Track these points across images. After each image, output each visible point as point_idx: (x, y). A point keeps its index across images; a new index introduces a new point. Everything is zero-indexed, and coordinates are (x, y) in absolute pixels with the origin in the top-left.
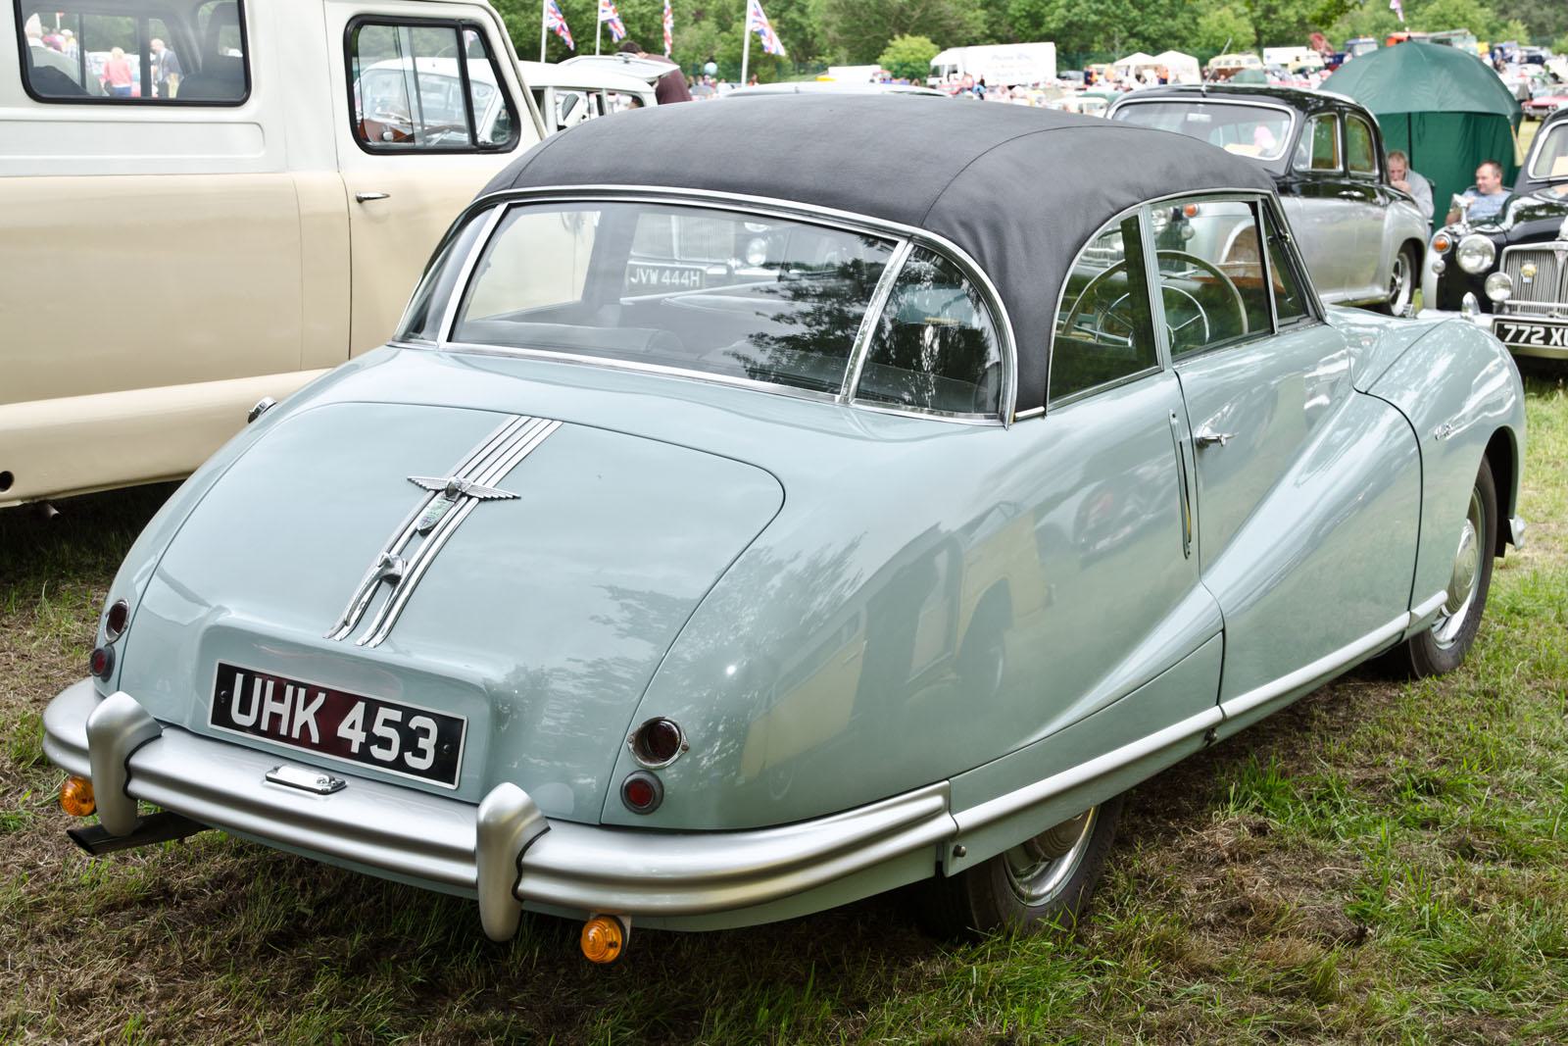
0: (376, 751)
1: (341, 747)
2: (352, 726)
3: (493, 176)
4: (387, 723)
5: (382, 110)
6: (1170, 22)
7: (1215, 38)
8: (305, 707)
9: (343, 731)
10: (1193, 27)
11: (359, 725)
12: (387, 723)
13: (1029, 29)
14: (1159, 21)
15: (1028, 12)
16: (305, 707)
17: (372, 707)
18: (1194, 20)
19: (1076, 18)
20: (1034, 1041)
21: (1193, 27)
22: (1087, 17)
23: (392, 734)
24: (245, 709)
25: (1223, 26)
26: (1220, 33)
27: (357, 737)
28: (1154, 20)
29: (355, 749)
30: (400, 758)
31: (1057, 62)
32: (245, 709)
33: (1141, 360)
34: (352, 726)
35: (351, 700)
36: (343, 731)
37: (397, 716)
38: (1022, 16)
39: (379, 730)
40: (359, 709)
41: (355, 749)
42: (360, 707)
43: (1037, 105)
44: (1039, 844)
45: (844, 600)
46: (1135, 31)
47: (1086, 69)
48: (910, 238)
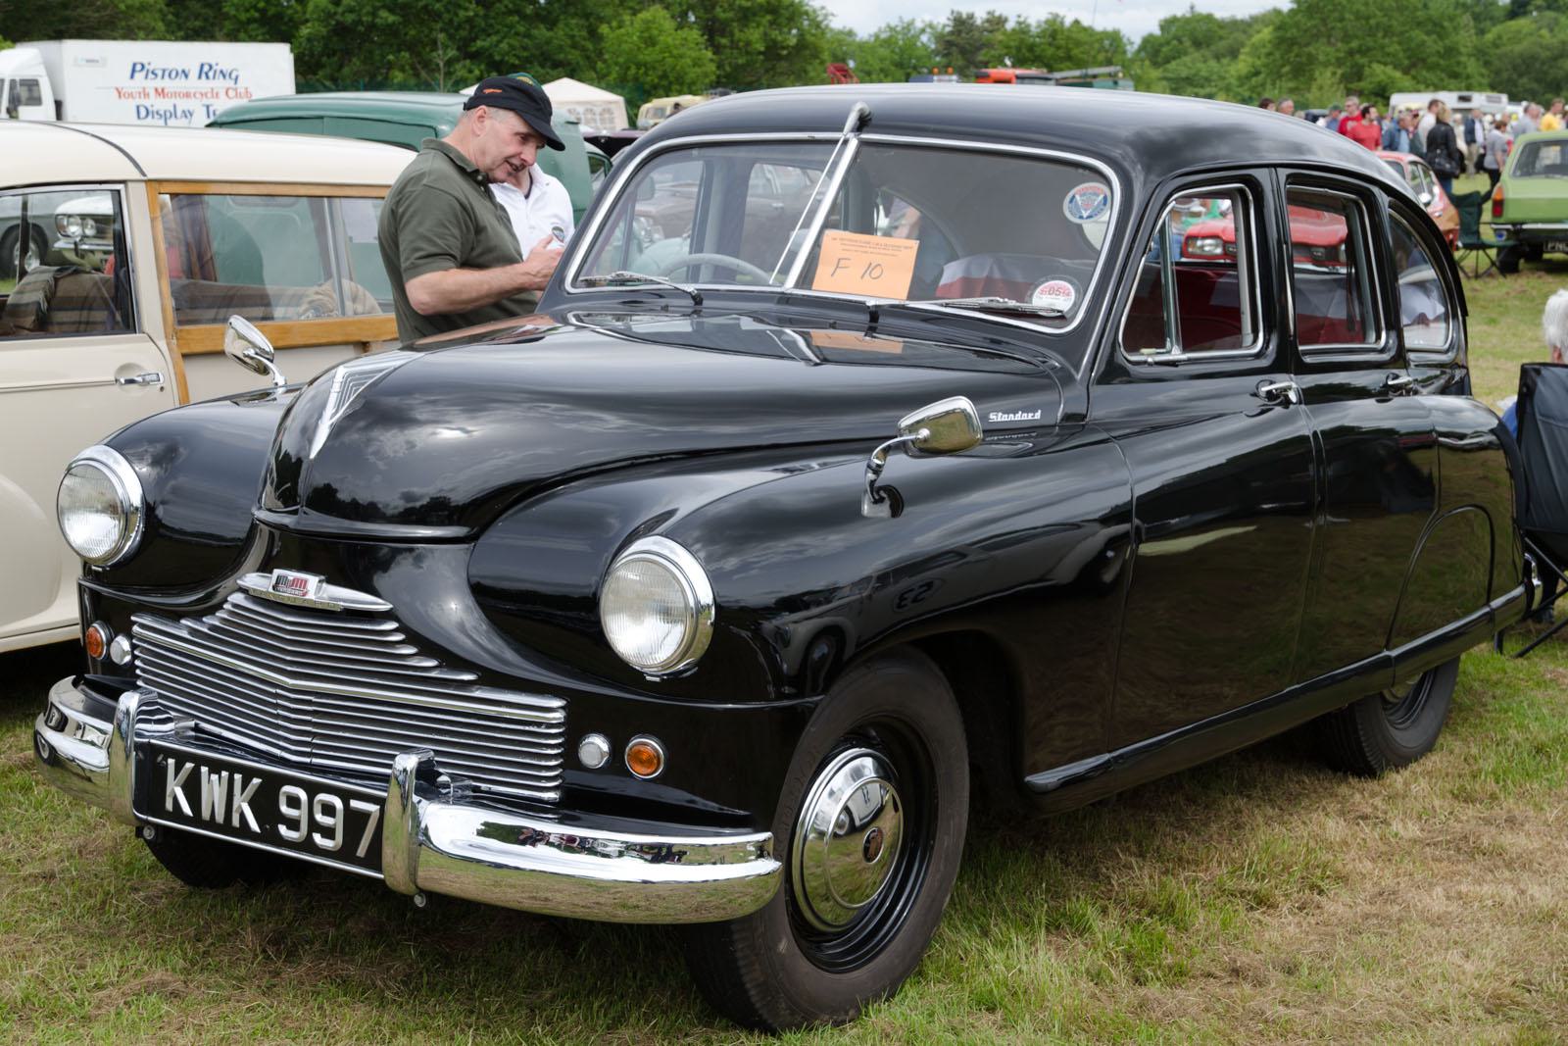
3: (397, 177)
5: (68, 487)
6: (541, 32)
7: (639, 65)
10: (589, 46)
13: (272, 27)
14: (521, 29)
15: (263, 12)
18: (593, 34)
19: (350, 18)
21: (589, 46)
22: (374, 14)
25: (651, 42)
26: (648, 55)
28: (511, 27)
30: (309, 837)
31: (297, 72)
38: (250, 21)
43: (1423, 207)
45: (56, 268)
46: (473, 49)
47: (630, 84)
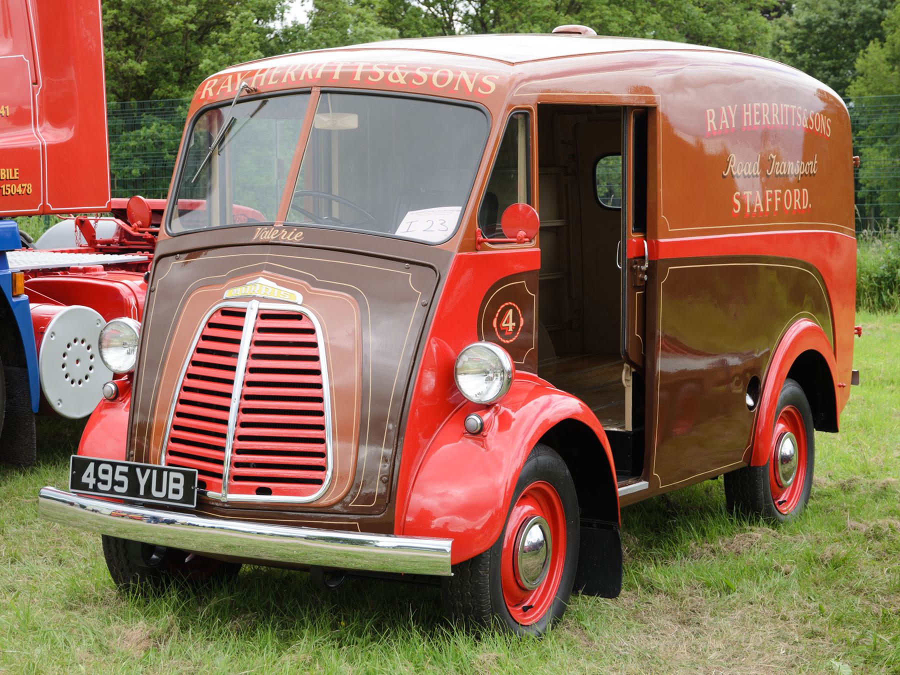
0: (100, 486)
1: (85, 487)
2: (89, 476)
4: (121, 473)
8: (143, 476)
9: (84, 479)
11: (92, 475)
12: (121, 473)
16: (143, 476)
17: (98, 463)
20: (895, 60)
23: (125, 479)
24: (159, 489)
27: (91, 481)
29: (91, 487)
30: (112, 489)
32: (159, 489)
33: (446, 29)
34: (89, 476)
35: (86, 463)
36: (84, 479)
37: (126, 469)
39: (118, 478)
40: (92, 466)
41: (91, 487)
42: (92, 465)
44: (644, 257)
48: (747, 218)
